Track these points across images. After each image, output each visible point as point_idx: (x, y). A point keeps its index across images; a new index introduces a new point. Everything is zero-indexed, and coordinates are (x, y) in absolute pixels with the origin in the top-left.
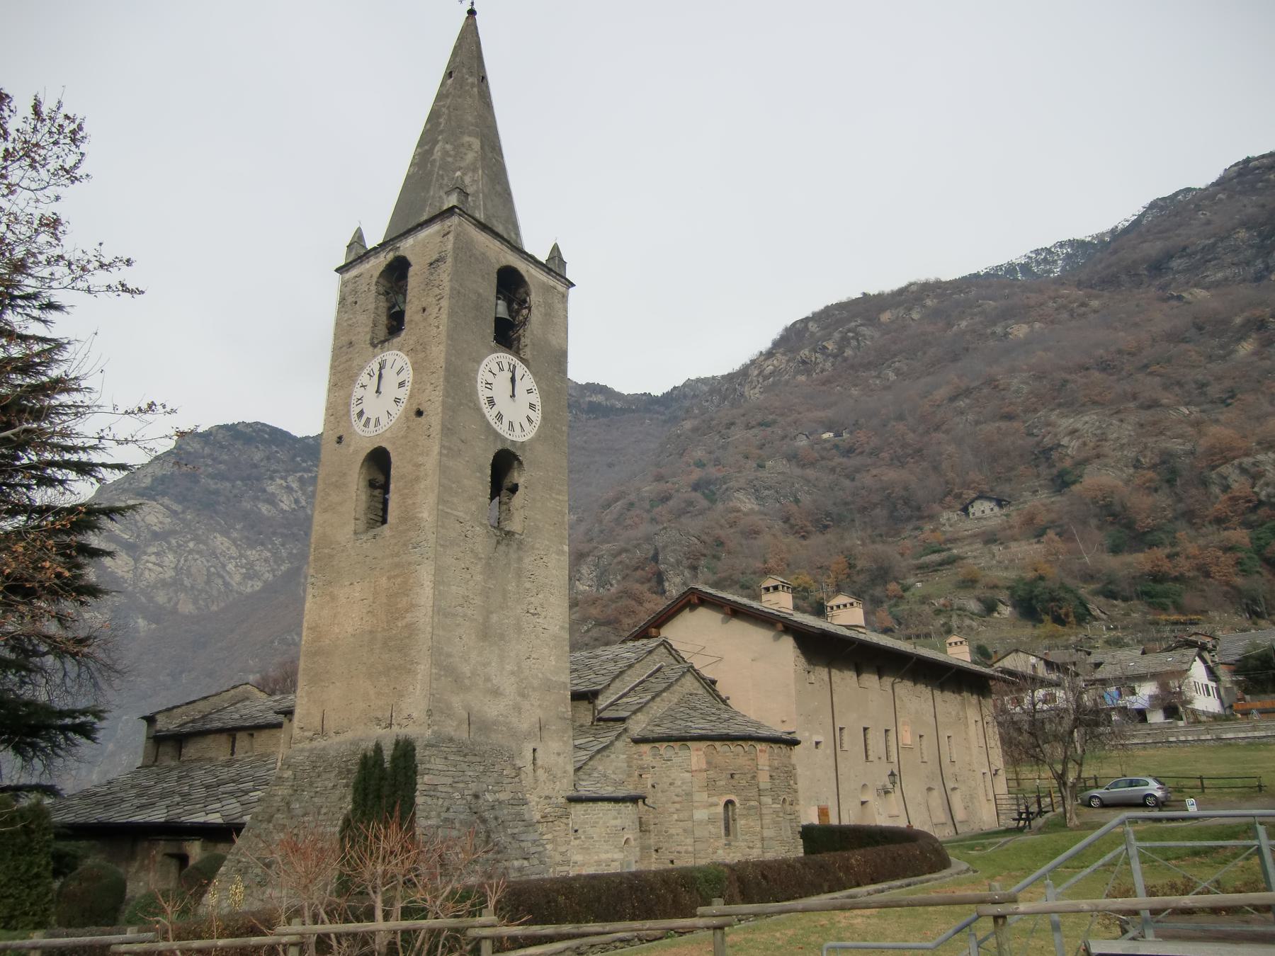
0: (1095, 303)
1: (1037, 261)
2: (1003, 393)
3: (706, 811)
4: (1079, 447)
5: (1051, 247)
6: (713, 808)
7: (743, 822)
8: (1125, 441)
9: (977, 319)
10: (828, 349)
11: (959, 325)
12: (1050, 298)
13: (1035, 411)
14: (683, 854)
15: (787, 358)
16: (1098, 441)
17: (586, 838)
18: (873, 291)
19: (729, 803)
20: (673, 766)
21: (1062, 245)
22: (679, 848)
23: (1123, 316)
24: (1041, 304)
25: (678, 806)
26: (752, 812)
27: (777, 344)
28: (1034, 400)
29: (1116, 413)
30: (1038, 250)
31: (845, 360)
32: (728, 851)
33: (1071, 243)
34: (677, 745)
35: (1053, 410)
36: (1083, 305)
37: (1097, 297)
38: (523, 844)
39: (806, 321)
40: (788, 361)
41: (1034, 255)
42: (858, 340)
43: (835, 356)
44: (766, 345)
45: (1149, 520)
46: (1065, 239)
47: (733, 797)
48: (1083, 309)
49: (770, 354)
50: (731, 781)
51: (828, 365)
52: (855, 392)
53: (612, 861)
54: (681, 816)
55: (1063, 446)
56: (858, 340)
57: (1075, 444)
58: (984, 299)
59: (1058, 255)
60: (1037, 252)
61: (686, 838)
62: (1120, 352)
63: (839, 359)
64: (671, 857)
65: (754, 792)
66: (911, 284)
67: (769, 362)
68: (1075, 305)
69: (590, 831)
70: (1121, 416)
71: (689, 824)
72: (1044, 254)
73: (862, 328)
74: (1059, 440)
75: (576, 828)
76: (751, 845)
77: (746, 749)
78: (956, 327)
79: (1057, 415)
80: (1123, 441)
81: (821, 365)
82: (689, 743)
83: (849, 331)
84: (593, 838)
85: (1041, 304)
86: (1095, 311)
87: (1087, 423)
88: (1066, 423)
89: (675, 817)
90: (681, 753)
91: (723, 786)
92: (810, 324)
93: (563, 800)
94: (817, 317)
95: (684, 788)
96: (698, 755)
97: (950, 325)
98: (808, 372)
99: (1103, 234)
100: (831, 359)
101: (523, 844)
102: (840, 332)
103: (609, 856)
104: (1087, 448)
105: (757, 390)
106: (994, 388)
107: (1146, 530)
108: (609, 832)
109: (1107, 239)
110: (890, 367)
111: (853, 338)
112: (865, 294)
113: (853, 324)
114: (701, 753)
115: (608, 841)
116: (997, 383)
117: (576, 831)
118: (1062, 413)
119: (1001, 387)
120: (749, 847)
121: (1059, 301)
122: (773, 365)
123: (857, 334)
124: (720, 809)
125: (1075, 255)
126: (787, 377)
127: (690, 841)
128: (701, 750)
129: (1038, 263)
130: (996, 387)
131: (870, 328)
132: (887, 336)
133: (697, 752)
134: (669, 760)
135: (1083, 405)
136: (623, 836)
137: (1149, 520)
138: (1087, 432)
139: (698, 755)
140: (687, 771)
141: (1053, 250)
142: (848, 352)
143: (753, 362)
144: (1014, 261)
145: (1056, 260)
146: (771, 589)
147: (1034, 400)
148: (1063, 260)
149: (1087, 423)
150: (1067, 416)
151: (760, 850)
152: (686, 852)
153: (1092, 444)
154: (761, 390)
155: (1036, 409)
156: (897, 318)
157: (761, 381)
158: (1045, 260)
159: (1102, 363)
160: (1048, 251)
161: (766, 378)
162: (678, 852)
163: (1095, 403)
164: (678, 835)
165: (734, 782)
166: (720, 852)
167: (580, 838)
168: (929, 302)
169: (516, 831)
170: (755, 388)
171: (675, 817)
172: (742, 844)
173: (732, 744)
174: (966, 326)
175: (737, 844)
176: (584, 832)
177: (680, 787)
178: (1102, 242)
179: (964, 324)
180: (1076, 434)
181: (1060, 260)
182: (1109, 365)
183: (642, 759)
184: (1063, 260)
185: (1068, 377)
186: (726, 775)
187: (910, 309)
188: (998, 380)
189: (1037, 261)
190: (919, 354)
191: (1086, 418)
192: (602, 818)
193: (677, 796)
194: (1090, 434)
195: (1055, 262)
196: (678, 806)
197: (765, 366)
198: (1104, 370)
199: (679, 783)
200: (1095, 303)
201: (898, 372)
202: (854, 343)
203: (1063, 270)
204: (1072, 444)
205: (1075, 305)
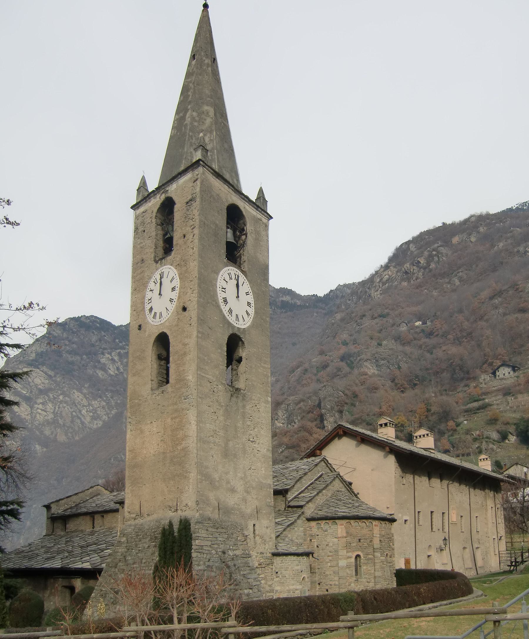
3: (345, 561)
7: (365, 567)
9: (509, 241)
10: (420, 263)
11: (498, 246)
15: (397, 270)
17: (282, 576)
18: (449, 222)
19: (358, 556)
20: (328, 535)
22: (331, 583)
26: (370, 561)
27: (391, 260)
31: (431, 271)
39: (408, 243)
40: (397, 272)
43: (425, 268)
44: (384, 260)
47: (360, 553)
49: (386, 267)
50: (359, 543)
58: (514, 227)
61: (334, 577)
63: (427, 270)
64: (327, 588)
65: (371, 550)
66: (472, 216)
67: (386, 273)
71: (336, 568)
73: (442, 248)
75: (277, 571)
78: (496, 247)
81: (416, 275)
82: (337, 521)
83: (434, 250)
84: (286, 577)
89: (329, 564)
91: (355, 546)
93: (270, 555)
95: (334, 547)
97: (493, 246)
98: (408, 280)
101: (249, 580)
102: (429, 251)
103: (294, 587)
105: (378, 292)
108: (294, 573)
111: (436, 255)
112: (444, 223)
113: (436, 245)
114: (343, 527)
116: (518, 287)
117: (277, 573)
120: (368, 582)
123: (438, 253)
124: (353, 560)
127: (336, 578)
128: (343, 525)
130: (517, 289)
131: (446, 248)
134: (326, 531)
136: (301, 576)
142: (433, 266)
146: (383, 425)
152: (335, 585)
154: (381, 292)
156: (462, 241)
162: (331, 585)
164: (330, 575)
165: (360, 544)
166: (353, 585)
167: (279, 577)
169: (245, 572)
171: (329, 564)
172: (364, 580)
174: (503, 247)
177: (332, 547)
179: (501, 245)
183: (312, 531)
186: (356, 540)
187: (470, 234)
190: (474, 266)
192: (290, 565)
196: (330, 558)
197: (384, 275)
201: (461, 280)
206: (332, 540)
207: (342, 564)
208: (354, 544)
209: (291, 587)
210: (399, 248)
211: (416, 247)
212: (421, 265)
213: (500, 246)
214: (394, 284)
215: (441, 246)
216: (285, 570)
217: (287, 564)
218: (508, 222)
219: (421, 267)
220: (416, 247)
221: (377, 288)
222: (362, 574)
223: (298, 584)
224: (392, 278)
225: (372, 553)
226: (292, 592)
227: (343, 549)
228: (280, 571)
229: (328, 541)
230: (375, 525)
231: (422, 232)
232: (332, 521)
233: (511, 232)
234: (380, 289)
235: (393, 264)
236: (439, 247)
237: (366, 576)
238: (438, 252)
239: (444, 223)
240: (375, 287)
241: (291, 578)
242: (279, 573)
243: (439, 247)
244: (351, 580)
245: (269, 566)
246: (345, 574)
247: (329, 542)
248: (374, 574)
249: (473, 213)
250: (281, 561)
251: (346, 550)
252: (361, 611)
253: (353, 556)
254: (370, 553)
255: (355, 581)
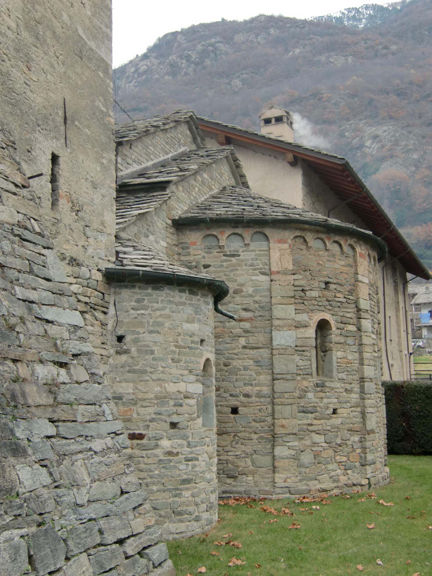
0: (394, 48)
1: (348, 17)
2: (325, 103)
3: (293, 333)
4: (378, 148)
5: (359, 8)
6: (302, 330)
7: (340, 354)
8: (411, 147)
9: (308, 48)
10: (192, 57)
11: (294, 51)
12: (362, 39)
13: (348, 120)
14: (253, 399)
15: (158, 61)
16: (392, 145)
17: (138, 351)
18: (229, 18)
20: (239, 265)
21: (367, 7)
22: (248, 389)
23: (412, 59)
24: (356, 44)
25: (247, 325)
26: (350, 341)
27: (151, 50)
28: (348, 111)
29: (407, 126)
30: (349, 9)
31: (204, 68)
32: (321, 395)
33: (375, 7)
34: (247, 234)
35: (361, 120)
36: (386, 48)
37: (395, 44)
38: (53, 330)
39: (175, 34)
40: (160, 64)
41: (346, 12)
42: (216, 54)
43: (197, 64)
44: (142, 51)
45: (425, 205)
46: (370, 3)
47: (327, 316)
48: (385, 51)
49: (145, 56)
50: (326, 293)
51: (191, 69)
52: (210, 93)
53: (186, 397)
54: (252, 340)
55: (367, 146)
56: (216, 54)
57: (376, 146)
58: (314, 34)
59: (363, 15)
60: (349, 10)
61: (258, 373)
62: (411, 83)
63: (200, 66)
64: (234, 402)
65: (351, 314)
66: (261, 15)
67: (144, 62)
68: (380, 47)
69: (148, 338)
70: (410, 129)
71: (265, 353)
72: (354, 12)
73: (221, 45)
74: (364, 142)
75: (120, 332)
76: (348, 387)
77: (346, 248)
78: (291, 53)
79: (364, 124)
80: (409, 148)
81: (185, 70)
82: (268, 231)
83: (210, 45)
84: (152, 352)
85: (356, 44)
86: (393, 54)
87: (385, 131)
88: (370, 130)
89: (242, 341)
90: (253, 245)
91: (315, 299)
92: (179, 37)
93: (99, 276)
94: (184, 32)
95: (257, 298)
96: (280, 250)
97: (287, 51)
98: (174, 74)
99: (396, 4)
100: (193, 65)
101: (53, 330)
102: (203, 45)
103: (182, 386)
104: (384, 149)
105: (132, 84)
106: (319, 100)
107: (421, 211)
108: (181, 343)
109: (399, 8)
110: (239, 77)
111: (212, 51)
112: (223, 19)
113: (213, 40)
114: (286, 246)
115: (179, 361)
116: (321, 96)
117: (120, 339)
118: (367, 123)
119: (324, 99)
120: (346, 390)
121: (369, 42)
122: (147, 65)
123: (215, 49)
124: (311, 332)
125: (375, 16)
126: (157, 76)
127: (265, 378)
128: (286, 242)
129: (349, 19)
130: (320, 99)
131: (226, 45)
132: (238, 53)
133: (280, 245)
134: (233, 256)
135: (384, 118)
136: (201, 355)
137: (425, 205)
138: (385, 138)
139: (280, 250)
140: (264, 274)
141: (360, 10)
142: (208, 62)
143: (131, 62)
144: (332, 14)
145: (362, 19)
146: (273, 121)
147: (348, 111)
148: (366, 19)
149: (385, 131)
150: (371, 126)
151: (357, 396)
152: (259, 395)
153: (387, 147)
154: (136, 84)
155: (348, 118)
156: (247, 40)
157: (136, 77)
158: (354, 16)
159: (398, 90)
160: (357, 10)
161: (140, 75)
162: (247, 396)
163: (391, 118)
164: (246, 368)
166: (310, 395)
167: (126, 352)
168: (272, 31)
169: (33, 295)
170: (130, 82)
171: (242, 341)
172: (338, 385)
173: (329, 238)
174: (299, 53)
175: (332, 385)
176: (136, 341)
177: (251, 296)
178: (395, 9)
179: (297, 51)
180: (377, 139)
181: (365, 19)
182: (402, 92)
183: (189, 254)
184: (366, 19)
185: (374, 97)
186: (318, 284)
187: (257, 35)
188: (323, 94)
189: (348, 17)
190: (261, 70)
191: (385, 128)
192: (168, 317)
193: (245, 310)
194: (386, 140)
195: (360, 20)
196: (247, 325)
197: (141, 65)
198: (398, 95)
199: (250, 290)
200: (394, 48)
201: (244, 81)
202: (212, 55)
203: (366, 25)
204: (373, 146)
205: (380, 47)
206: (254, 278)
207: (283, 342)
208: (315, 294)
209: (171, 388)
210: (162, 38)
211: (185, 39)
212: (193, 59)
213: (296, 52)
214: (154, 77)
215: (220, 42)
216: (151, 332)
217: (158, 313)
218: (306, 28)
219: (193, 62)
220: (185, 39)
221: (130, 79)
222: (335, 370)
223: (193, 378)
224: (152, 70)
225: (355, 321)
226: (172, 403)
227: (283, 301)
228: (134, 332)
229: (240, 280)
230: (361, 255)
231: (193, 25)
232: (251, 231)
233: (310, 39)
234: (135, 81)
235: (154, 55)
236: (217, 42)
237: (343, 376)
238: (216, 49)
239: (223, 19)
240: (128, 77)
241: (170, 356)
242: (128, 338)
243: (217, 42)
244: (305, 383)
245: (96, 314)
246: (292, 368)
247: (243, 285)
248: (360, 371)
249: (262, 13)
250: (138, 301)
251: (293, 307)
252: (221, 467)
253: (311, 322)
254: (351, 321)
255: (317, 385)
